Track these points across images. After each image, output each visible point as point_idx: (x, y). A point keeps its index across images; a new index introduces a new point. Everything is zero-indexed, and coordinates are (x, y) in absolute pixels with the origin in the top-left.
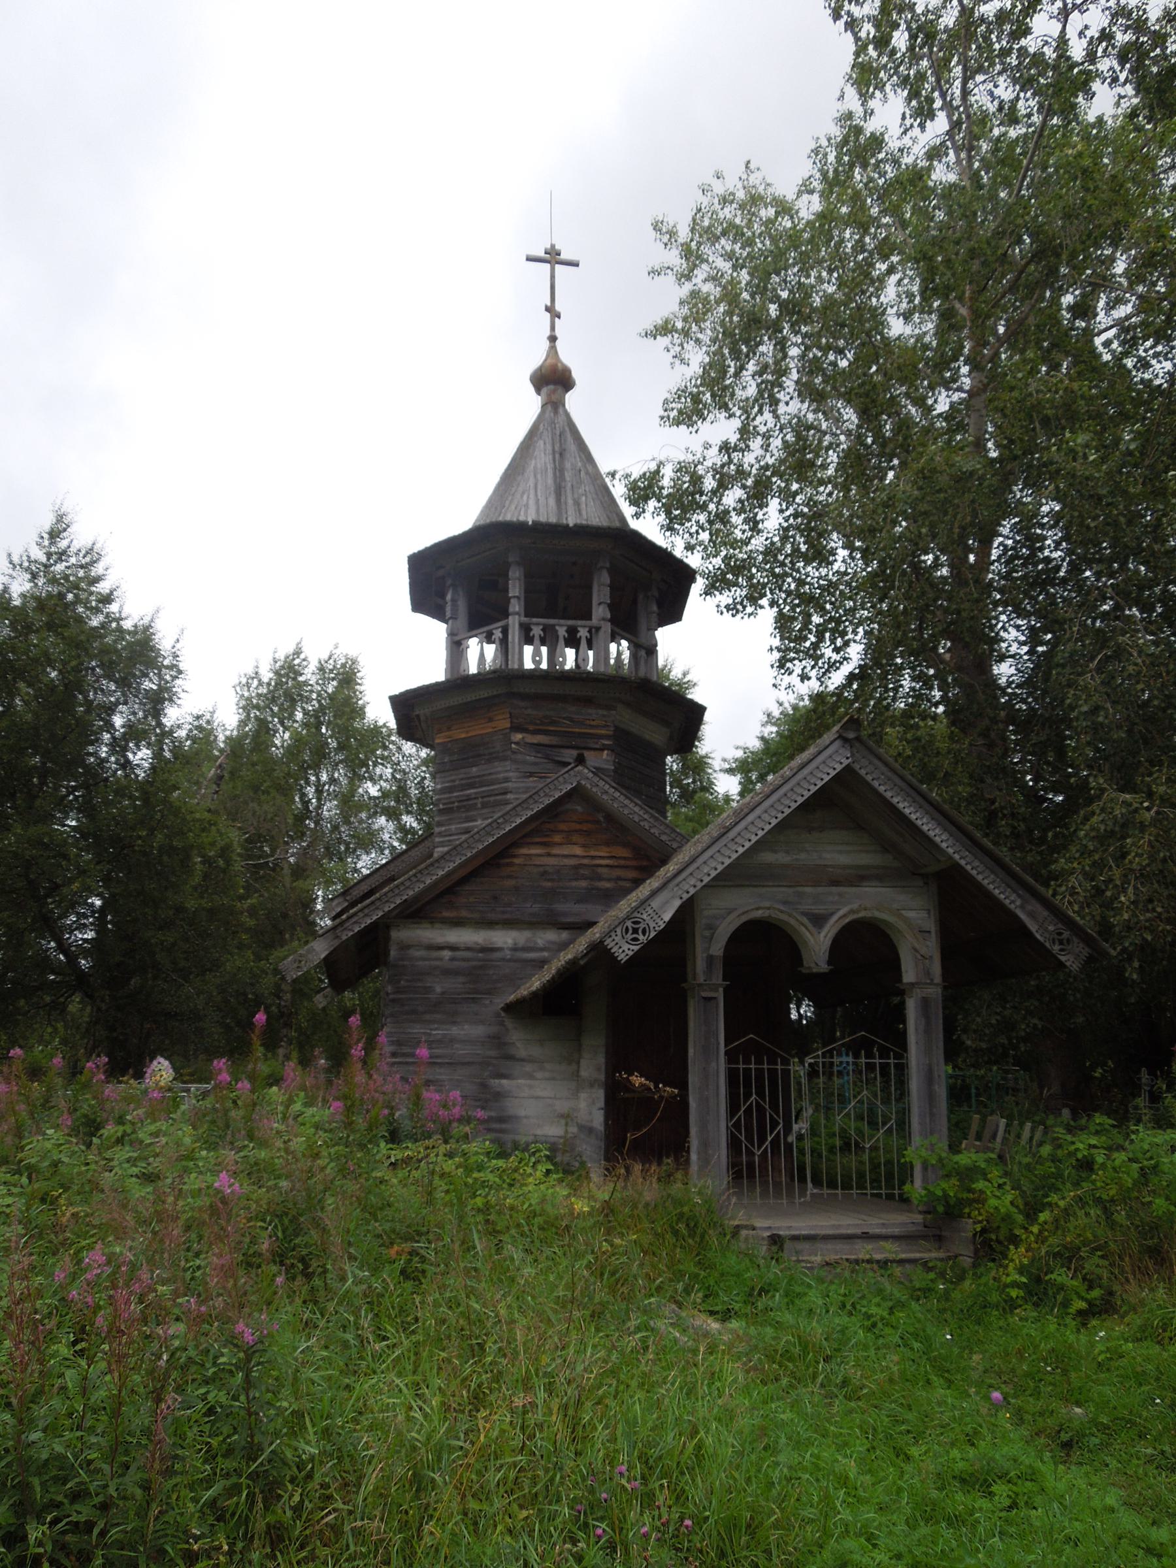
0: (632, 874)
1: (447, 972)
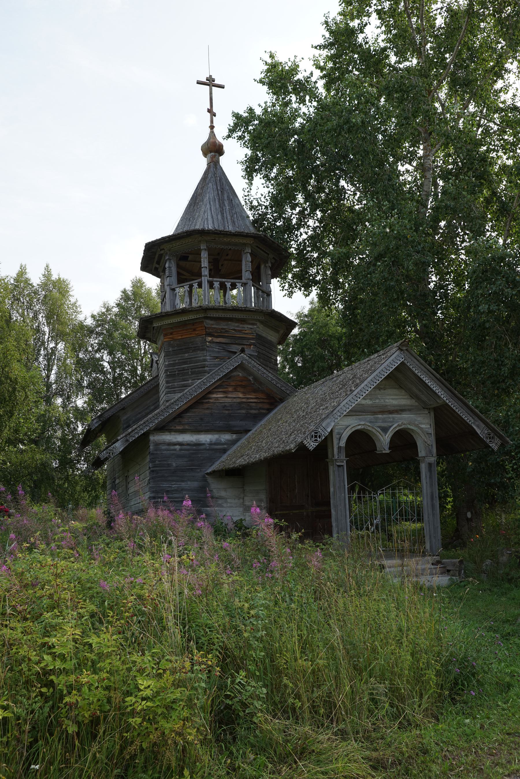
0: (267, 406)
1: (179, 456)
